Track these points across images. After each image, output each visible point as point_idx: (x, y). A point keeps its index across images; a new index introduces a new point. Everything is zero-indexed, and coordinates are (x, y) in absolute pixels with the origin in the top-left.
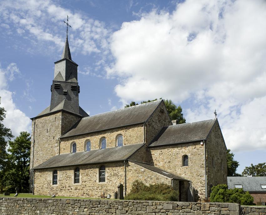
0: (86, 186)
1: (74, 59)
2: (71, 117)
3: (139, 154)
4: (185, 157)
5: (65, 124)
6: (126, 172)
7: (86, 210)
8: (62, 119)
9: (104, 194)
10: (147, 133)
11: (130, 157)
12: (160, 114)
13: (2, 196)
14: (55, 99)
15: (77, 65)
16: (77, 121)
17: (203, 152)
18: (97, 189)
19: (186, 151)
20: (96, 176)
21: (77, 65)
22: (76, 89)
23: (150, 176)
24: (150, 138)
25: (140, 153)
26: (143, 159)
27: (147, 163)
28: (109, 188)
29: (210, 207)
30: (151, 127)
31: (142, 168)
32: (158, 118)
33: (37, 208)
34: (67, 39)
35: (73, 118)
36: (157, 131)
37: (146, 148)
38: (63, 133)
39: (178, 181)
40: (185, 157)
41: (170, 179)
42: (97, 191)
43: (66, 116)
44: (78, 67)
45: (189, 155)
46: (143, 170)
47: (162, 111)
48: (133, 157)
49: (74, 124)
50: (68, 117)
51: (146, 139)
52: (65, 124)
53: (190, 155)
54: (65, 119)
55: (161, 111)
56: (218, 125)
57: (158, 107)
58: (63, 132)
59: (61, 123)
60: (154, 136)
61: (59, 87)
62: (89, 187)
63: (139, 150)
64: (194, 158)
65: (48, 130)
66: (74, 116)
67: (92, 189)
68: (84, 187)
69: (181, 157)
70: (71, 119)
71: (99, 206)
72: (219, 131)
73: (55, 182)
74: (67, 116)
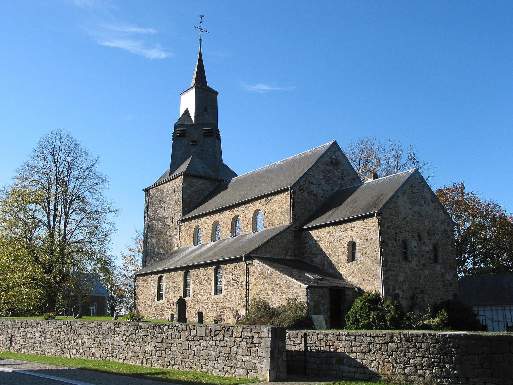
0: (197, 302)
1: (211, 83)
2: (200, 183)
3: (279, 243)
4: (352, 246)
5: (190, 196)
6: (248, 276)
7: (125, 337)
8: (184, 189)
9: (221, 316)
10: (296, 204)
11: (256, 250)
12: (329, 169)
13: (3, 319)
15: (217, 93)
16: (212, 189)
17: (377, 235)
18: (212, 307)
19: (353, 235)
20: (210, 284)
21: (217, 93)
22: (214, 134)
23: (278, 282)
24: (302, 214)
25: (280, 241)
26: (287, 253)
27: (297, 258)
28: (228, 304)
29: (242, 331)
30: (306, 193)
31: (268, 269)
33: (80, 336)
35: (204, 184)
36: (323, 199)
37: (295, 231)
38: (184, 213)
39: (326, 290)
40: (352, 246)
41: (305, 286)
42: (211, 309)
43: (191, 182)
45: (357, 241)
46: (269, 272)
47: (334, 162)
48: (264, 251)
49: (207, 193)
51: (294, 217)
52: (190, 196)
53: (358, 240)
54: (188, 187)
55: (332, 162)
56: (420, 181)
57: (322, 157)
59: (181, 195)
60: (315, 208)
61: (184, 133)
62: (202, 303)
63: (278, 237)
64: (365, 246)
65: (166, 208)
66: (205, 181)
67: (206, 307)
68: (195, 304)
69: (346, 246)
70: (200, 186)
71: (137, 331)
72: (426, 190)
73: (160, 297)
74: (193, 182)
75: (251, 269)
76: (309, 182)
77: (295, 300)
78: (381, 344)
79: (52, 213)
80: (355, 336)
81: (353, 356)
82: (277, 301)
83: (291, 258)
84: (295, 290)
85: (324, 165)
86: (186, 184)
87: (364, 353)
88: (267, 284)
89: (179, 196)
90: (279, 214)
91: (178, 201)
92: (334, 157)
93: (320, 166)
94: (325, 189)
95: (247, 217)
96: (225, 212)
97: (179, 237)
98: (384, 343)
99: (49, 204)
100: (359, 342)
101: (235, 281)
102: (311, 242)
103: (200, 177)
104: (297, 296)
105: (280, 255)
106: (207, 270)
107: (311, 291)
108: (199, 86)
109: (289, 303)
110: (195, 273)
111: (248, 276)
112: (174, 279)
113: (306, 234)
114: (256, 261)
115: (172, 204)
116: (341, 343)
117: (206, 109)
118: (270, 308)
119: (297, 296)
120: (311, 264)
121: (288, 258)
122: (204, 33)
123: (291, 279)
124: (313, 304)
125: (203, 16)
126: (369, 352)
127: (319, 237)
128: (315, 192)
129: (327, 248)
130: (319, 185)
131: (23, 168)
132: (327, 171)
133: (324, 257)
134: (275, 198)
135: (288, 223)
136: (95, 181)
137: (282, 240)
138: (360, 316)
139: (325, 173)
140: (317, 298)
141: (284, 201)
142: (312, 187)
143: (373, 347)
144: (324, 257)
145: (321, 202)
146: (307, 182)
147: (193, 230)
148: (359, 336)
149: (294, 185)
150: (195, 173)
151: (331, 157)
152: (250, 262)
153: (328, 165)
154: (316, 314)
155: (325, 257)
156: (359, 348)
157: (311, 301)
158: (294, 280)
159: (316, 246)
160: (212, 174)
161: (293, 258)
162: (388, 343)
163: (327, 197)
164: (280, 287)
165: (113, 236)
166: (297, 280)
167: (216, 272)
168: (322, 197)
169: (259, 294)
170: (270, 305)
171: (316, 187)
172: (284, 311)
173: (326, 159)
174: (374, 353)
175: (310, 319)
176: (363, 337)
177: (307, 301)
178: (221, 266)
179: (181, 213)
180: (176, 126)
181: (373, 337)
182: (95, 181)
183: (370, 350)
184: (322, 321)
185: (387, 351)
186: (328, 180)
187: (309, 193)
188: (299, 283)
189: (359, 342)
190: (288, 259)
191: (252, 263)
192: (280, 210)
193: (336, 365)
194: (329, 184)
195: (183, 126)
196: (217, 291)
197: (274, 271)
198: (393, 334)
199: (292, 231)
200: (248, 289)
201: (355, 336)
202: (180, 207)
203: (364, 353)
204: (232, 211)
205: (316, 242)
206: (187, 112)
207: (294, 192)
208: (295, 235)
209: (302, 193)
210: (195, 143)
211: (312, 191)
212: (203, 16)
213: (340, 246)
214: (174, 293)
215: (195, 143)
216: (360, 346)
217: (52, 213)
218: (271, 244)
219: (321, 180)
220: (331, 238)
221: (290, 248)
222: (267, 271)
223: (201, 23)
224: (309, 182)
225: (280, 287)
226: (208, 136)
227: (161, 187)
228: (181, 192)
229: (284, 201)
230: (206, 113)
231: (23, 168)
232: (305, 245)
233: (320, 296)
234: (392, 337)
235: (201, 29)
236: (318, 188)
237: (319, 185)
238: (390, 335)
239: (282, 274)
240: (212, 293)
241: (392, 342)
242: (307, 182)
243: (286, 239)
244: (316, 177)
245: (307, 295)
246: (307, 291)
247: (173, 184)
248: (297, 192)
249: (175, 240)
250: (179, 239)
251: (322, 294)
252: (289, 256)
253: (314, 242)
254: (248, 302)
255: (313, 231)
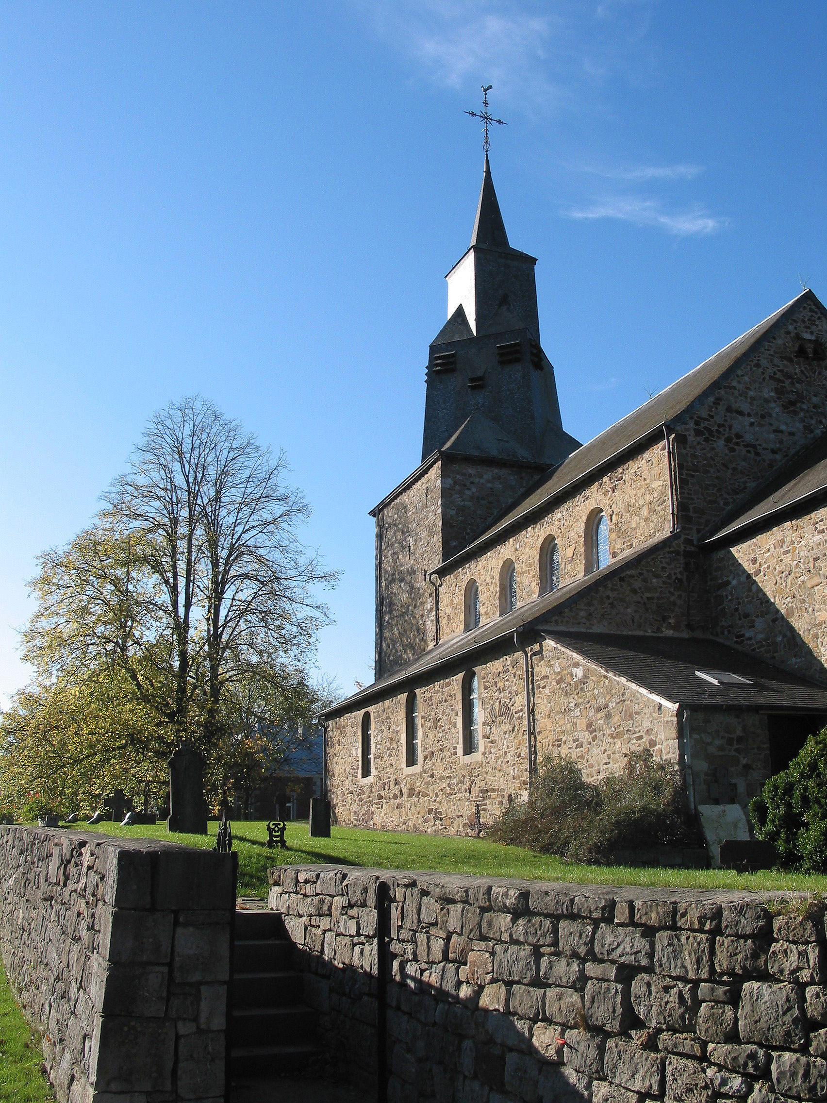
1: (517, 240)
3: (634, 591)
6: (531, 692)
8: (445, 493)
10: (685, 477)
14: (441, 414)
15: (534, 261)
21: (534, 261)
23: (602, 701)
25: (637, 584)
26: (664, 619)
27: (698, 634)
30: (721, 443)
31: (577, 665)
32: (779, 392)
34: (488, 172)
35: (499, 478)
36: (778, 457)
37: (687, 554)
41: (671, 707)
43: (464, 475)
44: (537, 268)
46: (579, 672)
47: (810, 350)
50: (477, 480)
51: (684, 512)
54: (457, 487)
55: (801, 352)
58: (454, 543)
59: (440, 511)
61: (452, 363)
62: (442, 778)
65: (412, 548)
66: (504, 472)
68: (428, 783)
70: (489, 485)
73: (366, 773)
75: (541, 669)
76: (729, 409)
77: (647, 754)
78: (696, 983)
79: (182, 582)
80: (556, 918)
81: (544, 1039)
82: (602, 763)
83: (677, 635)
84: (647, 724)
85: (776, 361)
86: (450, 481)
87: (597, 1031)
88: (577, 712)
89: (434, 515)
90: (645, 512)
91: (435, 525)
92: (807, 336)
93: (764, 362)
94: (783, 427)
95: (572, 534)
96: (524, 532)
97: (437, 615)
98: (713, 977)
99: (174, 567)
100: (575, 955)
101: (506, 711)
102: (734, 582)
103: (488, 462)
104: (653, 743)
105: (639, 626)
106: (448, 684)
107: (694, 719)
108: (483, 246)
109: (631, 767)
110: (428, 695)
111: (531, 692)
112: (388, 718)
113: (721, 560)
114: (549, 643)
115: (424, 534)
116: (493, 954)
117: (504, 301)
118: (583, 786)
119: (653, 743)
120: (739, 648)
121: (669, 633)
122: (479, 109)
123: (633, 686)
124: (702, 766)
125: (490, 87)
126: (624, 1033)
127: (754, 561)
128: (748, 438)
129: (780, 591)
130: (763, 417)
131: (114, 489)
132: (788, 376)
133: (774, 621)
134: (633, 466)
135: (666, 532)
136: (278, 509)
137: (645, 580)
138: (805, 801)
139: (779, 381)
140: (721, 748)
141: (654, 470)
142: (740, 424)
143: (654, 1002)
144: (774, 621)
145: (771, 466)
146: (722, 408)
147: (463, 592)
148: (573, 917)
149: (679, 418)
150: (475, 453)
151: (798, 337)
152: (536, 647)
153: (790, 360)
154: (717, 802)
155: (778, 623)
156: (576, 998)
157: (692, 756)
158: (644, 691)
159: (750, 590)
160: (523, 453)
161: (685, 635)
162: (736, 981)
163: (792, 451)
164: (608, 716)
165: (323, 635)
166: (652, 688)
167: (467, 689)
168: (774, 452)
169: (558, 743)
170: (584, 779)
171: (752, 424)
172: (617, 795)
173: (780, 342)
174: (651, 1045)
175: (693, 821)
176: (596, 923)
177: (681, 756)
178: (477, 669)
179: (440, 556)
180: (433, 349)
181: (649, 932)
182: (278, 509)
183: (631, 1021)
184: (736, 826)
185: (732, 1037)
186: (792, 403)
187: (728, 440)
188: (657, 699)
189: (575, 955)
190: (667, 639)
191: (540, 652)
192: (648, 498)
193: (476, 1085)
194: (795, 413)
195: (450, 345)
196: (469, 747)
197: (592, 665)
198: (769, 917)
199: (678, 553)
200: (532, 733)
201: (556, 918)
202: (437, 540)
203: (597, 1031)
204: (538, 526)
205: (749, 576)
206: (460, 312)
207: (681, 440)
208: (687, 565)
209: (706, 440)
210: (478, 384)
211: (738, 436)
212: (490, 87)
213: (816, 580)
214: (390, 755)
215: (478, 384)
216: (580, 983)
217: (182, 582)
218: (609, 593)
219: (767, 401)
220: (787, 560)
221: (674, 604)
222: (575, 670)
223: (486, 103)
224: (729, 409)
225: (608, 716)
226: (510, 362)
227: (404, 498)
228: (440, 502)
229: (656, 470)
230: (504, 308)
231: (114, 489)
232: (719, 593)
233: (730, 742)
234: (764, 937)
235: (486, 118)
236: (760, 425)
237: (763, 417)
238: (748, 925)
239: (610, 674)
240: (460, 751)
241: (764, 976)
242: (722, 408)
243: (657, 576)
244: (751, 393)
245: (681, 735)
246: (680, 725)
247: (424, 487)
248: (691, 438)
249: (430, 626)
250: (437, 621)
251: (739, 732)
252: (670, 626)
253: (743, 579)
254: (533, 770)
255: (738, 547)
